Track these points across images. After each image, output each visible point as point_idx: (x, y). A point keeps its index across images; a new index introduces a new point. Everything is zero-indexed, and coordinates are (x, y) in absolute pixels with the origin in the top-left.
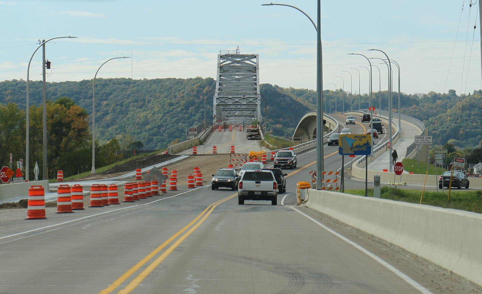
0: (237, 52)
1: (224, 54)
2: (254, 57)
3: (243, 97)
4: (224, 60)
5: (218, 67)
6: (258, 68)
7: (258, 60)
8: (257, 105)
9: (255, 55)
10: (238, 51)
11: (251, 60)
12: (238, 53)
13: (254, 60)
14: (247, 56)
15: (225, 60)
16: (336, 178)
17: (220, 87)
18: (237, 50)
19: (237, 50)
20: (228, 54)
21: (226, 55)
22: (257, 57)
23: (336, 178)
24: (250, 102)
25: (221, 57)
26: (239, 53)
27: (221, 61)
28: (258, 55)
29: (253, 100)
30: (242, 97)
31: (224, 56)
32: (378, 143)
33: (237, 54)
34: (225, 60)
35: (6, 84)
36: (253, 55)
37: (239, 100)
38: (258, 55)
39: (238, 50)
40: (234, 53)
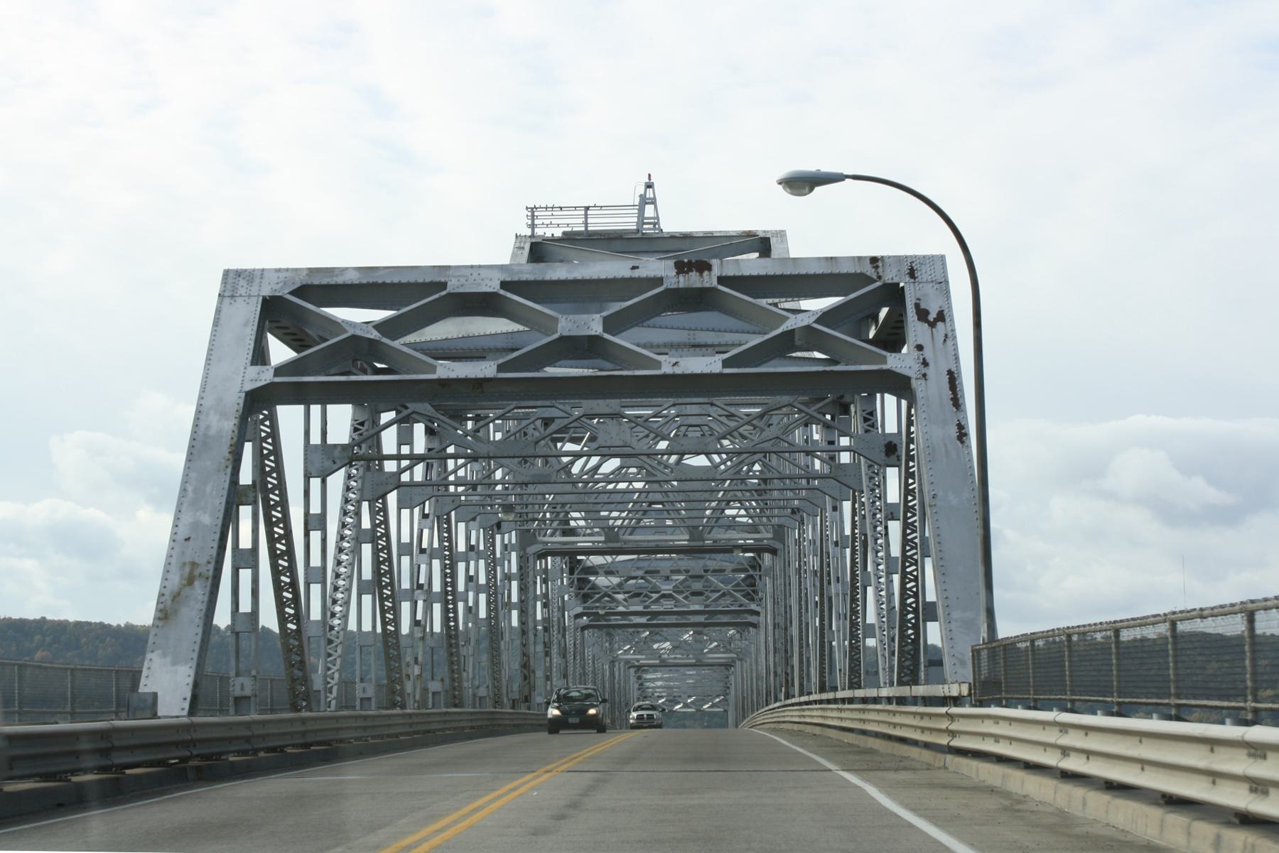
1: (558, 233)
3: (684, 281)
9: (762, 235)
10: (649, 211)
30: (658, 281)
37: (613, 324)
40: (627, 222)
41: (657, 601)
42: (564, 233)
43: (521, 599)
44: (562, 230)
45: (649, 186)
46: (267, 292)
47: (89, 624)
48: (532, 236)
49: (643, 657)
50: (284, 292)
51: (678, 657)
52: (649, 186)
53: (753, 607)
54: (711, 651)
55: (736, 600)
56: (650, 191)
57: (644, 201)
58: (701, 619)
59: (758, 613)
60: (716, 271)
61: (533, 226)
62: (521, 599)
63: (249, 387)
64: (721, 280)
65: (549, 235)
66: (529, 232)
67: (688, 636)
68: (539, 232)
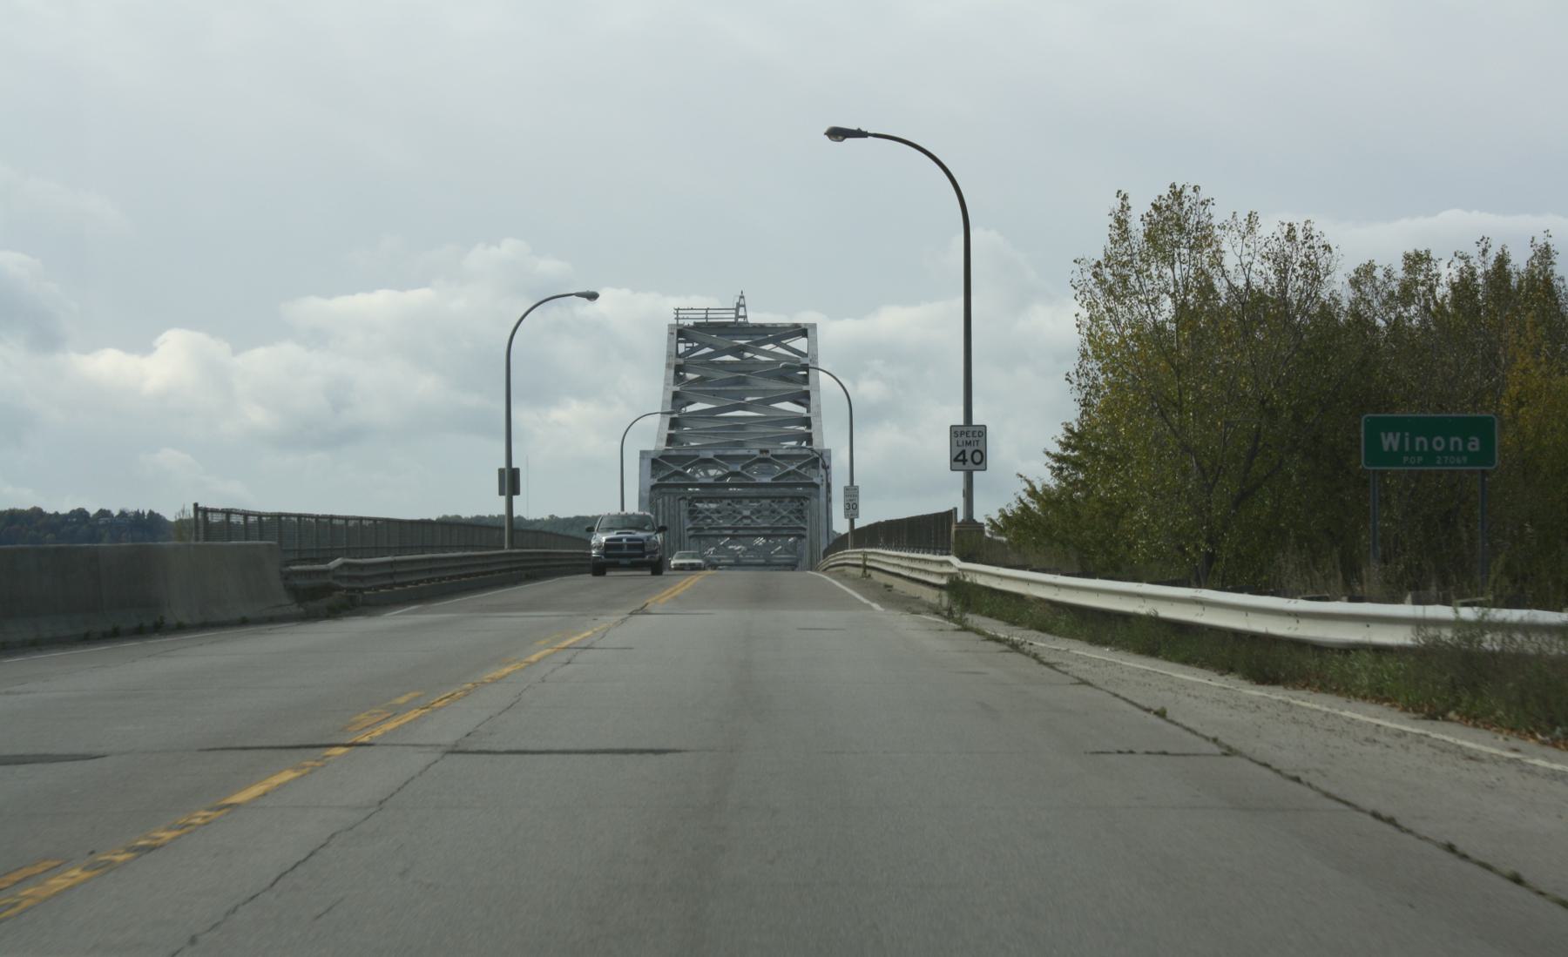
0: (738, 316)
1: (691, 323)
2: (801, 331)
3: (761, 456)
4: (690, 345)
5: (668, 366)
6: (672, 334)
7: (813, 344)
8: (816, 486)
9: (803, 327)
10: (741, 313)
11: (790, 344)
12: (740, 320)
13: (800, 344)
14: (774, 328)
15: (696, 344)
16: (623, 509)
17: (673, 432)
18: (737, 310)
19: (737, 310)
20: (705, 321)
21: (697, 326)
22: (809, 332)
23: (623, 509)
24: (789, 473)
25: (682, 333)
26: (745, 317)
27: (682, 348)
28: (814, 326)
29: (799, 467)
30: (755, 456)
31: (689, 327)
32: (806, 461)
33: (740, 323)
34: (696, 344)
35: (13, 517)
36: (797, 326)
37: (743, 468)
38: (814, 326)
39: (742, 309)
40: (729, 317)
41: (741, 519)
42: (695, 323)
43: (945, 617)
44: (693, 321)
45: (742, 297)
46: (653, 457)
47: (36, 516)
48: (678, 325)
49: (724, 557)
50: (657, 457)
51: (750, 558)
52: (742, 297)
53: (802, 525)
54: (776, 553)
55: (791, 521)
56: (742, 300)
57: (739, 306)
58: (769, 532)
59: (804, 529)
60: (771, 453)
61: (677, 319)
62: (945, 617)
63: (652, 484)
64: (772, 455)
65: (686, 324)
66: (675, 322)
67: (760, 541)
68: (681, 322)
